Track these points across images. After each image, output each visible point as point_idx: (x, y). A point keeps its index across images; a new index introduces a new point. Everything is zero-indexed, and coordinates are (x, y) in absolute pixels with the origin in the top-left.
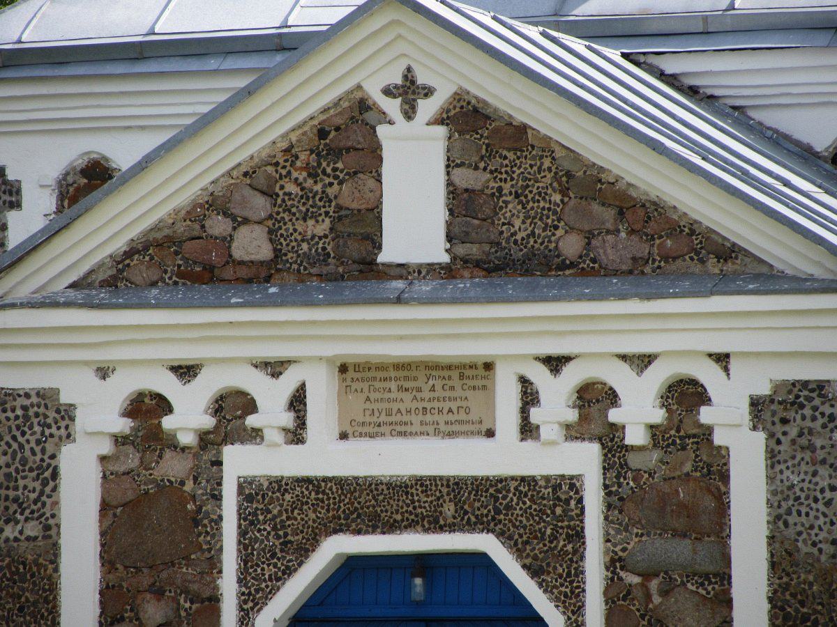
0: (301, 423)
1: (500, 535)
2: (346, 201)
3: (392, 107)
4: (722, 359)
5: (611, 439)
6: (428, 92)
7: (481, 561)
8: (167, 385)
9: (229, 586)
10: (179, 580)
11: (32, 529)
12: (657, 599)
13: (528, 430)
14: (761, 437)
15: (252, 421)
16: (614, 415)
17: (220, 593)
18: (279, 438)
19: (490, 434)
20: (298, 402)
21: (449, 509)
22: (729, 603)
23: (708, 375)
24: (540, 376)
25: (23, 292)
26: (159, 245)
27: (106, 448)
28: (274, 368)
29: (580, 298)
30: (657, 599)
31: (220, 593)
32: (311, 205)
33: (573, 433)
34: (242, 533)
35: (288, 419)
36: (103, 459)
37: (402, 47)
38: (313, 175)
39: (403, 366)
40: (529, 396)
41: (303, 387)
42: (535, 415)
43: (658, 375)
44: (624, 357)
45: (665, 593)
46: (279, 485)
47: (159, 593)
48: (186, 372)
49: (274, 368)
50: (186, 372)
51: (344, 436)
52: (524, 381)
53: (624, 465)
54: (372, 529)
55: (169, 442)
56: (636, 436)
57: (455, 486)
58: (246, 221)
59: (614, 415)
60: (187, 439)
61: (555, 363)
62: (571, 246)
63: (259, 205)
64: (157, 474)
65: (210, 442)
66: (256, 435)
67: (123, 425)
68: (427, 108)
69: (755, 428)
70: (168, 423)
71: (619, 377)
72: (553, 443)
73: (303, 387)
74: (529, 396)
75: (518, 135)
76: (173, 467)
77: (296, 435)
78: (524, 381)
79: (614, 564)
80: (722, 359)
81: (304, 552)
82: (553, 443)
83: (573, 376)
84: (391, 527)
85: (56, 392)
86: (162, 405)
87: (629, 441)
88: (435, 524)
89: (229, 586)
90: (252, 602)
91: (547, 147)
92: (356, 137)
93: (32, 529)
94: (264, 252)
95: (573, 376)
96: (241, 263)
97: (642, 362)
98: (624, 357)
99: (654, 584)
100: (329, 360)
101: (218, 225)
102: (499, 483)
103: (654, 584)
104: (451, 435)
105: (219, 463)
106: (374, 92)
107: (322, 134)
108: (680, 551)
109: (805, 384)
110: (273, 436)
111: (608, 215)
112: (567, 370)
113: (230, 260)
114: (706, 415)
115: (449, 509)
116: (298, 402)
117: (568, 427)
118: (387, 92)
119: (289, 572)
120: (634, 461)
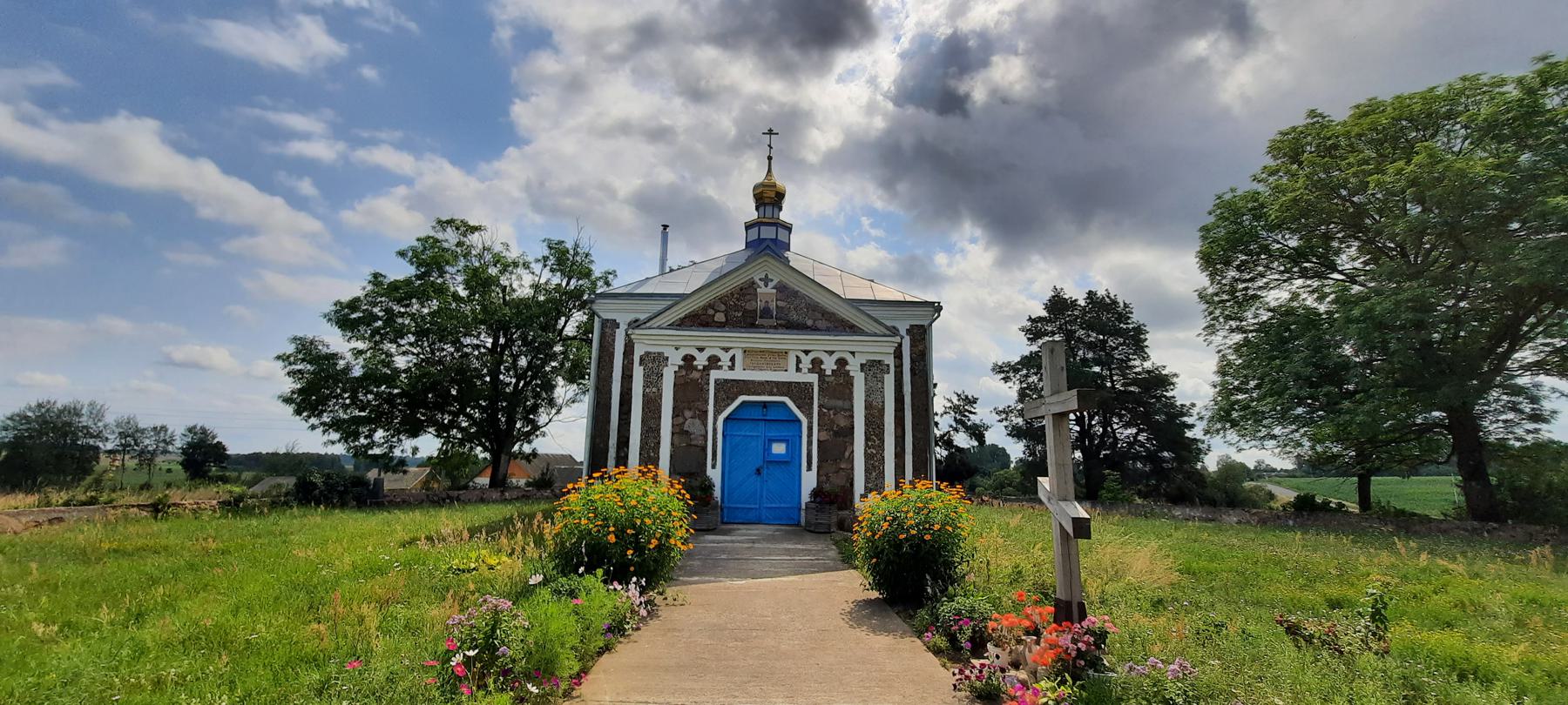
0: (733, 365)
1: (790, 397)
2: (747, 307)
3: (761, 284)
4: (853, 353)
5: (821, 373)
6: (772, 280)
7: (784, 404)
8: (695, 353)
9: (711, 408)
10: (1334, 306)
11: (654, 390)
12: (832, 416)
13: (798, 369)
14: (863, 374)
15: (720, 363)
16: (823, 367)
17: (1122, 305)
18: (727, 368)
19: (786, 370)
20: (733, 359)
21: (775, 390)
22: (853, 417)
23: (849, 357)
24: (802, 356)
25: (655, 326)
26: (693, 316)
27: (677, 369)
28: (726, 350)
29: (818, 335)
30: (832, 416)
31: (1122, 305)
32: (736, 308)
33: (810, 371)
34: (715, 394)
35: (730, 364)
36: (675, 372)
37: (766, 268)
38: (738, 300)
39: (763, 351)
40: (799, 361)
41: (734, 355)
42: (801, 366)
43: (835, 357)
44: (825, 351)
45: (834, 414)
46: (726, 381)
47: (690, 409)
48: (701, 350)
49: (726, 350)
50: (701, 350)
51: (744, 369)
52: (797, 357)
53: (824, 380)
54: (753, 394)
55: (695, 368)
56: (829, 372)
57: (777, 384)
58: (719, 311)
59: (823, 367)
60: (700, 367)
61: (807, 352)
62: (810, 323)
63: (723, 307)
64: (691, 376)
65: (706, 369)
66: (720, 368)
67: (682, 363)
68: (771, 285)
69: (861, 371)
70: (695, 363)
71: (824, 357)
72: (805, 373)
73: (734, 355)
74: (799, 361)
75: (796, 294)
76: (695, 375)
77: (732, 368)
78: (797, 357)
79: (820, 406)
80: (853, 353)
81: (733, 400)
82: (805, 373)
83: (812, 356)
84: (759, 394)
85: (663, 353)
86: (693, 358)
87: (827, 373)
88: (771, 394)
89: (711, 408)
90: (717, 413)
91: (804, 297)
92: (752, 291)
93: (654, 390)
94: (724, 320)
95: (812, 356)
96: (717, 322)
97: (831, 353)
98: (825, 351)
99: (831, 412)
100: (742, 348)
101: (711, 312)
102: (790, 383)
103: (831, 412)
104: (775, 370)
105: (709, 375)
106: (757, 279)
107: (741, 290)
108: (840, 403)
109: (875, 361)
110: (726, 368)
111: (820, 316)
112: (810, 354)
113: (714, 321)
114: (848, 368)
115: (775, 390)
116: (733, 359)
117: (809, 369)
118: (760, 279)
119: (729, 405)
120: (827, 379)
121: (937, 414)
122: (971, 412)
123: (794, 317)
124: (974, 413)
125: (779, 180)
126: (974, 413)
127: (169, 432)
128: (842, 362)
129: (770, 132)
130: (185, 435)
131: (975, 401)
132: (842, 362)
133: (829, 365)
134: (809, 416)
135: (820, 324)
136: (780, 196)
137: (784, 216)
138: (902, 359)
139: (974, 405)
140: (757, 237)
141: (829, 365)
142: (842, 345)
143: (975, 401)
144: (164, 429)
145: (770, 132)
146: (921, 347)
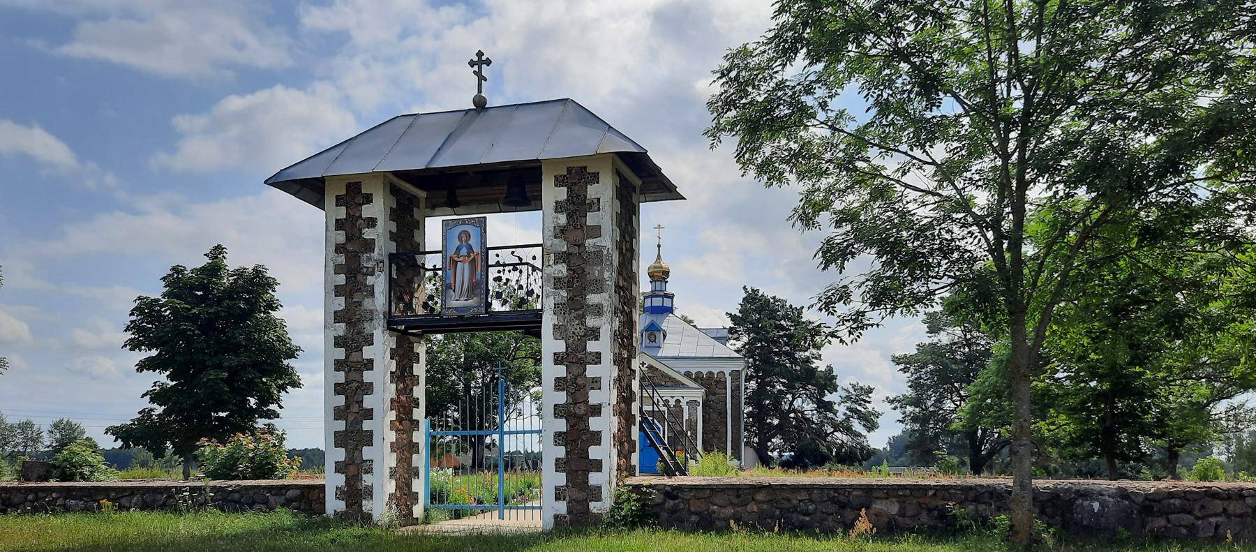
4: (683, 397)
23: (681, 399)
43: (675, 399)
62: (663, 383)
68: (645, 366)
71: (670, 399)
73: (685, 199)
80: (683, 397)
97: (673, 397)
114: (681, 404)
121: (835, 403)
122: (865, 401)
123: (656, 381)
124: (869, 402)
125: (665, 264)
126: (869, 402)
127: (35, 428)
128: (678, 401)
129: (659, 227)
130: (51, 432)
131: (870, 391)
132: (678, 401)
133: (672, 403)
134: (664, 426)
135: (668, 384)
136: (667, 273)
137: (670, 289)
138: (726, 390)
139: (870, 395)
140: (650, 305)
141: (672, 403)
142: (678, 393)
143: (870, 391)
144: (29, 425)
145: (659, 227)
146: (737, 383)
